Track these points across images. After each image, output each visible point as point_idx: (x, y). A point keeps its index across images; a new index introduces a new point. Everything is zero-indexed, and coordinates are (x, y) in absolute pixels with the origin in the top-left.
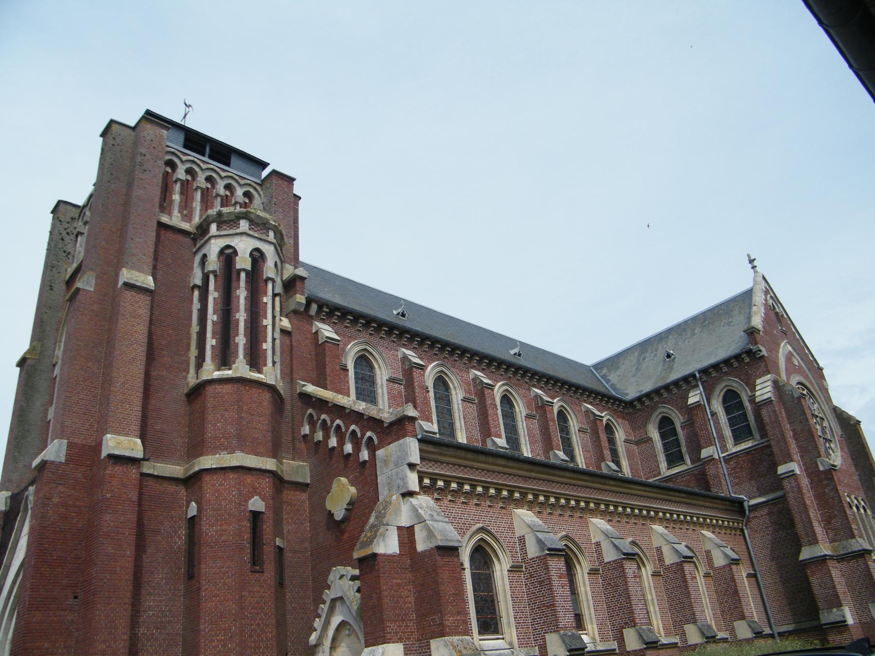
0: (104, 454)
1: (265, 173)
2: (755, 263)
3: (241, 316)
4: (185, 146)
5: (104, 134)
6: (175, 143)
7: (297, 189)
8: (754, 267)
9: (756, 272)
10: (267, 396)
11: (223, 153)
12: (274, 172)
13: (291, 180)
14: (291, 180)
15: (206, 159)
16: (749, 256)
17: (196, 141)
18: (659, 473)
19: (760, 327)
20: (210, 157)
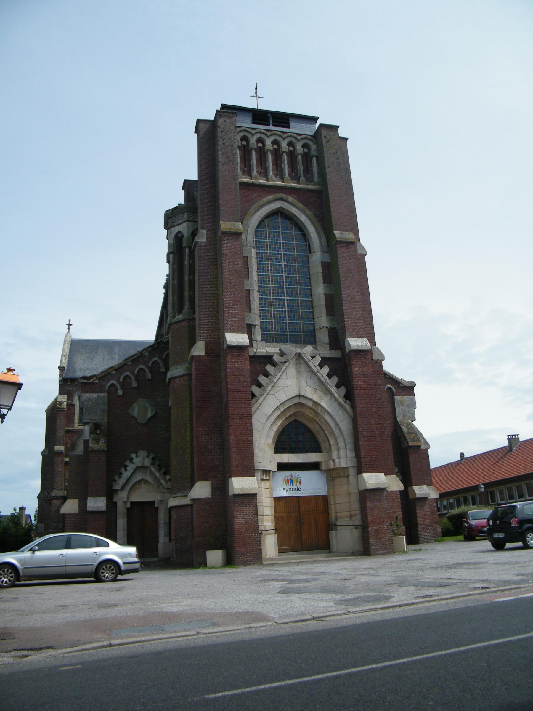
0: (225, 346)
1: (317, 125)
2: (71, 327)
3: (186, 294)
4: (254, 123)
5: (196, 131)
6: (246, 123)
7: (342, 133)
8: (69, 329)
9: (68, 332)
10: (10, 405)
11: (282, 119)
12: (321, 125)
13: (335, 128)
14: (335, 128)
15: (271, 128)
16: (70, 321)
17: (260, 116)
18: (73, 427)
19: (66, 366)
20: (274, 125)
